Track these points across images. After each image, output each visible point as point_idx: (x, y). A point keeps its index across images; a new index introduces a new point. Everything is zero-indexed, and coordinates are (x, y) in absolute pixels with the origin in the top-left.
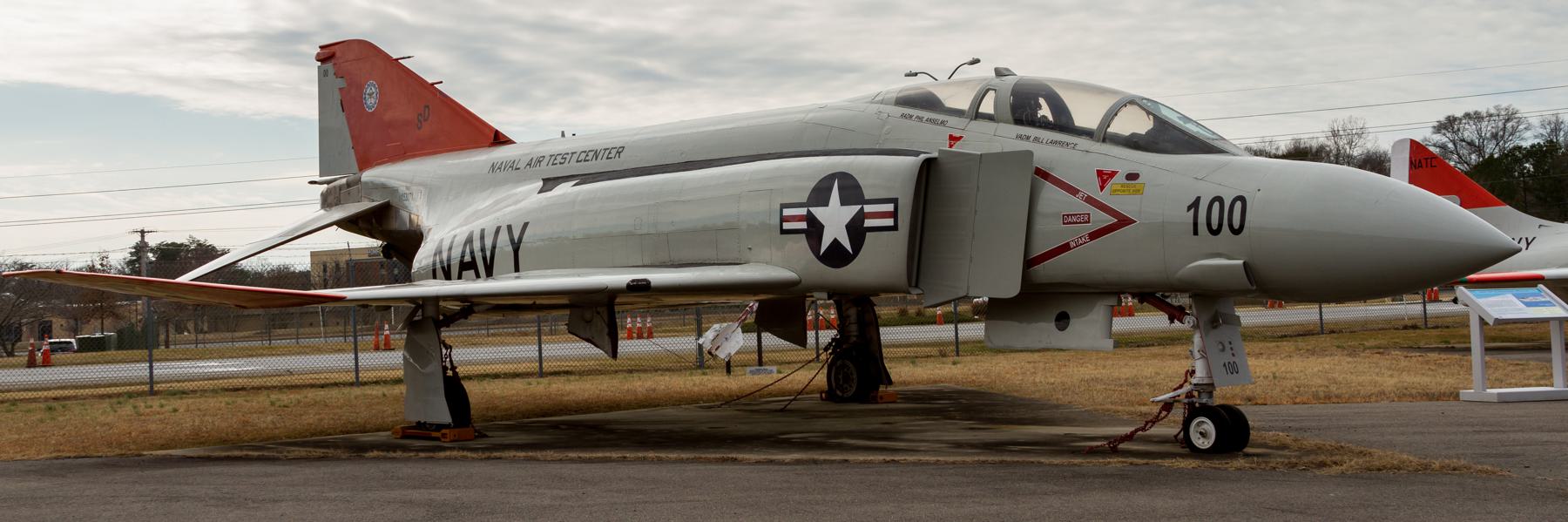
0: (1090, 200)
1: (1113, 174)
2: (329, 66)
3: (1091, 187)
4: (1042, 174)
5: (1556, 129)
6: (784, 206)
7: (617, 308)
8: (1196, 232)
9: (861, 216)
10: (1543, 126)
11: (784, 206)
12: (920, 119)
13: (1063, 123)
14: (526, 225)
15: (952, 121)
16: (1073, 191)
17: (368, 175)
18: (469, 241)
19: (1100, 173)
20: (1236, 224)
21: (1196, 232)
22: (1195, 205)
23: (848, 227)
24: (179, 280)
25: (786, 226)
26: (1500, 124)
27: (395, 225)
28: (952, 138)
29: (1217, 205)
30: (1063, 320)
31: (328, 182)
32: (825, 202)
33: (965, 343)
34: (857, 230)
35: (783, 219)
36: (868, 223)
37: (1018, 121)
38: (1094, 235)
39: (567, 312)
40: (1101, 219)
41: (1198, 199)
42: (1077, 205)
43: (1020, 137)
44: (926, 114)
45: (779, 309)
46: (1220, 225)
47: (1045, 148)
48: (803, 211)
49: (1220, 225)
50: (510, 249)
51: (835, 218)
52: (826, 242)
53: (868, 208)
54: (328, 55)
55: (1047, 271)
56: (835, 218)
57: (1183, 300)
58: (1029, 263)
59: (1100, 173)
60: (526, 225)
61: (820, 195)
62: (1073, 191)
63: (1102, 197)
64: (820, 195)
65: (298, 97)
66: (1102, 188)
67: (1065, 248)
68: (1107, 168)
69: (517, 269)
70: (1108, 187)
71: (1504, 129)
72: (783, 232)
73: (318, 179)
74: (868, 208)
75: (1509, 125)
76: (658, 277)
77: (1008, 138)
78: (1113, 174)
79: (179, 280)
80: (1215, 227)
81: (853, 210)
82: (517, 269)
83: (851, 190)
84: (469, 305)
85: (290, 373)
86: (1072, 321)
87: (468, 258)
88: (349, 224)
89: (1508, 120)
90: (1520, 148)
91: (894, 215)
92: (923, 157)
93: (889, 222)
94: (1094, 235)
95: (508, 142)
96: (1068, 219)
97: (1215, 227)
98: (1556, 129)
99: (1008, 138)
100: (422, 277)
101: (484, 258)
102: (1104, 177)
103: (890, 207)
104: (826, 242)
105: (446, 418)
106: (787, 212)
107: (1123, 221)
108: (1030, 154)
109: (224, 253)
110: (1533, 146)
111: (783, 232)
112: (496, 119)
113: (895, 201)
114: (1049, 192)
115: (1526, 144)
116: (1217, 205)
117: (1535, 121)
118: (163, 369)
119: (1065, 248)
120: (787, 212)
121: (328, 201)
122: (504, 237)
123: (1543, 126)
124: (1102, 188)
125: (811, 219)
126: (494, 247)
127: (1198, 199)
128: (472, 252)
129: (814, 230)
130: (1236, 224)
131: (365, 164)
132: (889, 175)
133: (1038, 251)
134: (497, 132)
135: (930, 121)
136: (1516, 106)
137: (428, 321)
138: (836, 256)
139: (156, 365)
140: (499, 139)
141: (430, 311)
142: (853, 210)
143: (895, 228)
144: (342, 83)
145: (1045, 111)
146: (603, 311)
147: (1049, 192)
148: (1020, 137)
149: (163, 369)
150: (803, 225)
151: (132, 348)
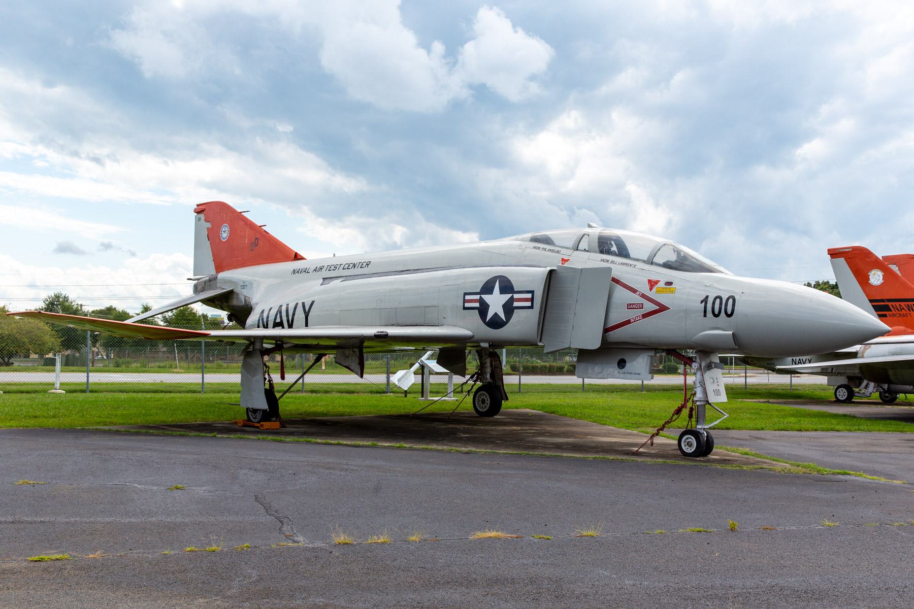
0: (643, 296)
1: (657, 282)
2: (202, 216)
3: (644, 289)
4: (615, 280)
6: (465, 294)
7: (365, 350)
8: (705, 316)
9: (512, 300)
11: (465, 294)
12: (545, 249)
13: (623, 252)
14: (313, 302)
15: (563, 251)
16: (634, 291)
17: (221, 275)
18: (280, 311)
19: (650, 281)
20: (729, 312)
21: (705, 316)
22: (705, 300)
23: (504, 306)
24: (125, 322)
25: (467, 305)
27: (235, 302)
28: (563, 260)
29: (718, 301)
30: (622, 364)
31: (198, 279)
32: (503, 291)
33: (382, 373)
34: (509, 308)
35: (465, 301)
36: (516, 304)
37: (602, 252)
38: (645, 316)
39: (335, 351)
40: (651, 307)
41: (707, 297)
42: (636, 299)
43: (603, 260)
44: (548, 247)
45: (452, 354)
46: (720, 312)
47: (618, 267)
48: (477, 297)
49: (720, 312)
50: (303, 316)
51: (496, 302)
52: (490, 315)
53: (516, 296)
54: (201, 210)
55: (616, 335)
56: (496, 302)
57: (691, 353)
58: (606, 330)
59: (650, 281)
60: (313, 302)
61: (488, 288)
62: (634, 291)
63: (652, 294)
64: (488, 288)
65: (187, 229)
66: (651, 289)
67: (628, 322)
68: (654, 278)
69: (307, 325)
70: (654, 289)
72: (465, 308)
73: (192, 277)
76: (393, 331)
77: (596, 261)
78: (657, 282)
79: (125, 322)
80: (716, 312)
81: (507, 297)
82: (307, 325)
83: (507, 287)
84: (280, 344)
85: (785, 403)
87: (278, 320)
88: (209, 302)
91: (532, 300)
92: (549, 269)
93: (529, 304)
94: (645, 316)
95: (302, 258)
96: (630, 306)
97: (716, 312)
99: (596, 261)
100: (252, 327)
101: (288, 321)
102: (652, 284)
103: (529, 296)
104: (490, 315)
105: (265, 406)
106: (467, 297)
107: (662, 308)
108: (610, 269)
109: (132, 317)
111: (465, 308)
112: (294, 246)
113: (532, 292)
114: (619, 291)
116: (718, 301)
118: (587, 381)
119: (628, 322)
120: (467, 297)
121: (196, 289)
122: (300, 310)
124: (651, 289)
125: (481, 301)
126: (294, 314)
127: (707, 297)
128: (281, 317)
129: (483, 309)
130: (729, 312)
131: (220, 268)
132: (529, 276)
133: (611, 324)
134: (296, 254)
135: (550, 250)
137: (253, 350)
138: (496, 323)
139: (90, 374)
140: (297, 257)
141: (258, 346)
142: (507, 297)
143: (531, 307)
144: (209, 225)
145: (614, 248)
146: (357, 350)
147: (619, 291)
148: (603, 260)
149: (587, 381)
150: (477, 305)
151: (860, 284)
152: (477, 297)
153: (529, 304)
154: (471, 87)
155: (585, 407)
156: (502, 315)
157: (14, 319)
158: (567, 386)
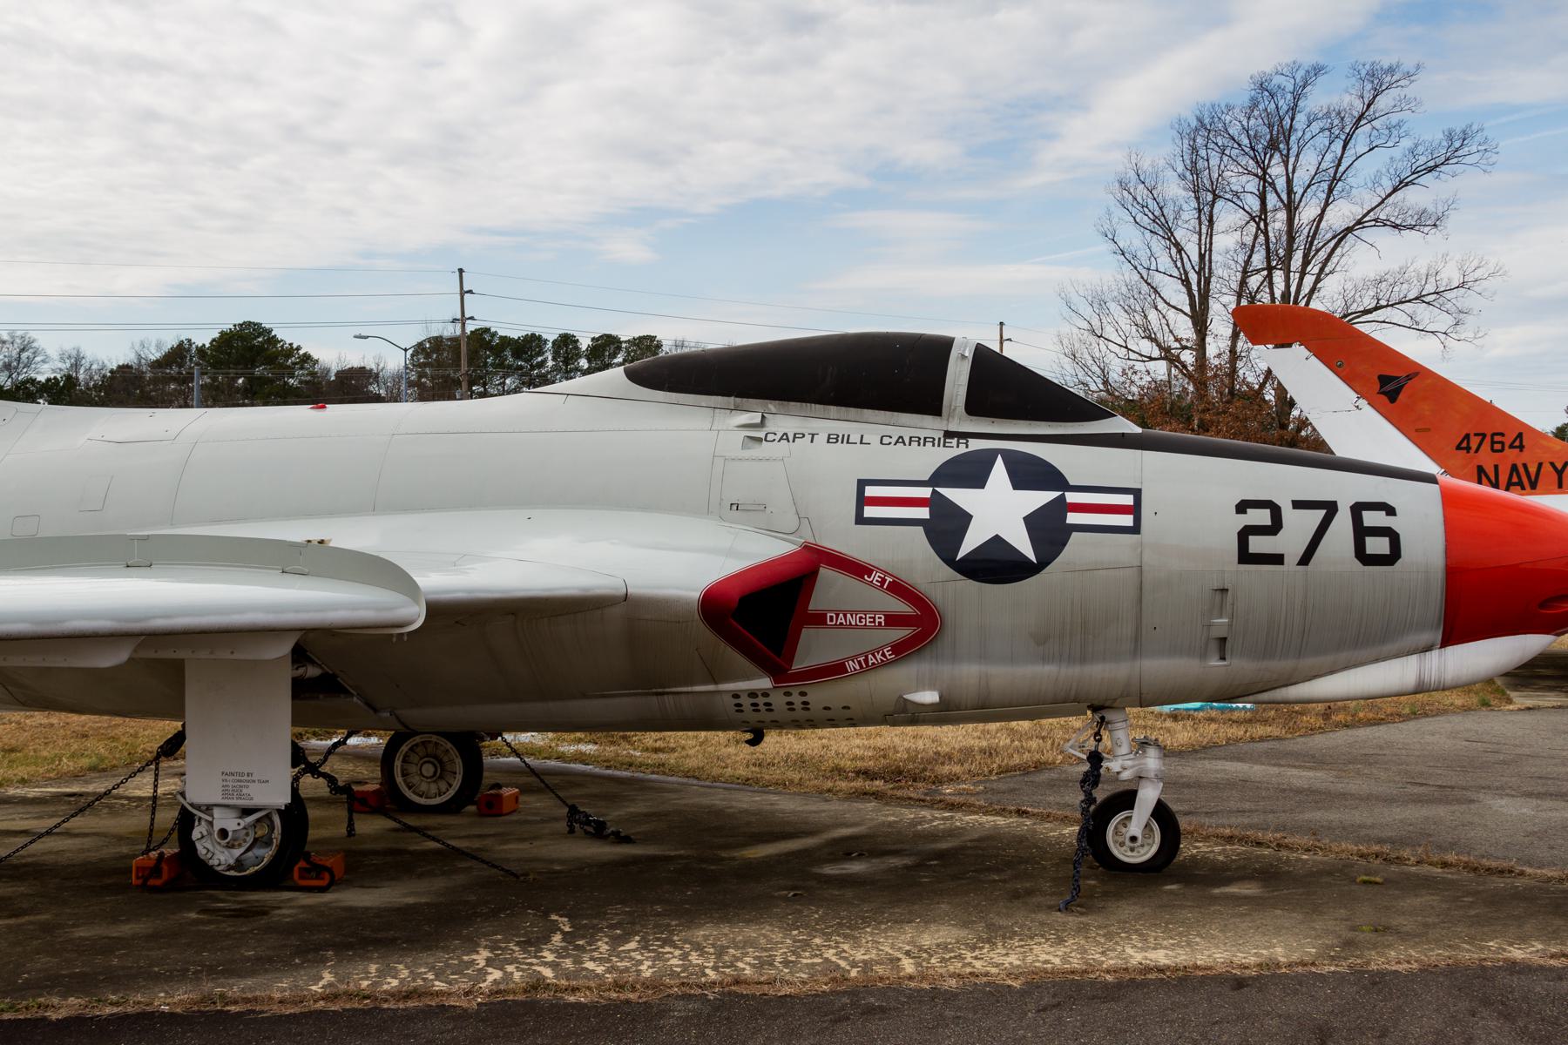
5: (76, 365)
6: (862, 484)
10: (62, 360)
26: (15, 354)
34: (1049, 530)
35: (862, 501)
36: (1073, 518)
52: (972, 540)
53: (1071, 497)
69: (1560, 486)
71: (19, 359)
72: (860, 520)
74: (1071, 497)
75: (24, 355)
81: (1040, 498)
82: (1560, 486)
86: (695, 594)
89: (23, 350)
90: (33, 381)
98: (76, 365)
101: (427, 828)
104: (972, 540)
110: (48, 380)
115: (42, 378)
117: (53, 352)
120: (870, 491)
123: (62, 360)
125: (936, 503)
129: (946, 526)
136: (33, 335)
142: (1040, 498)
150: (923, 513)
152: (925, 492)
153: (1127, 520)
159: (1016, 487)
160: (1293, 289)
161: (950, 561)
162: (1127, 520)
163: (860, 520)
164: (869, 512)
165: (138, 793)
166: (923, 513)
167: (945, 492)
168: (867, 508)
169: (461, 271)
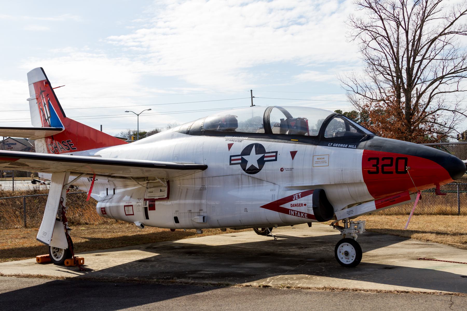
3: (422, 77)
6: (231, 156)
9: (264, 157)
34: (261, 162)
35: (231, 160)
36: (265, 159)
48: (240, 157)
52: (248, 166)
53: (266, 155)
72: (231, 164)
81: (260, 156)
104: (248, 166)
106: (232, 158)
120: (232, 158)
125: (243, 159)
129: (244, 162)
142: (260, 156)
150: (240, 161)
152: (240, 157)
154: (281, 120)
155: (315, 254)
156: (257, 166)
157: (263, 230)
158: (361, 130)
159: (249, 155)
160: (429, 43)
161: (260, 170)
162: (274, 158)
163: (231, 164)
164: (232, 162)
165: (302, 209)
166: (240, 161)
167: (244, 157)
168: (385, 168)
169: (251, 91)
